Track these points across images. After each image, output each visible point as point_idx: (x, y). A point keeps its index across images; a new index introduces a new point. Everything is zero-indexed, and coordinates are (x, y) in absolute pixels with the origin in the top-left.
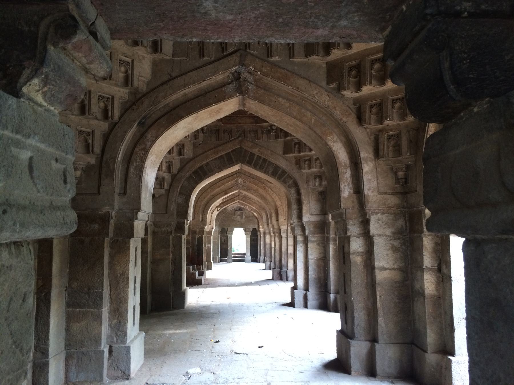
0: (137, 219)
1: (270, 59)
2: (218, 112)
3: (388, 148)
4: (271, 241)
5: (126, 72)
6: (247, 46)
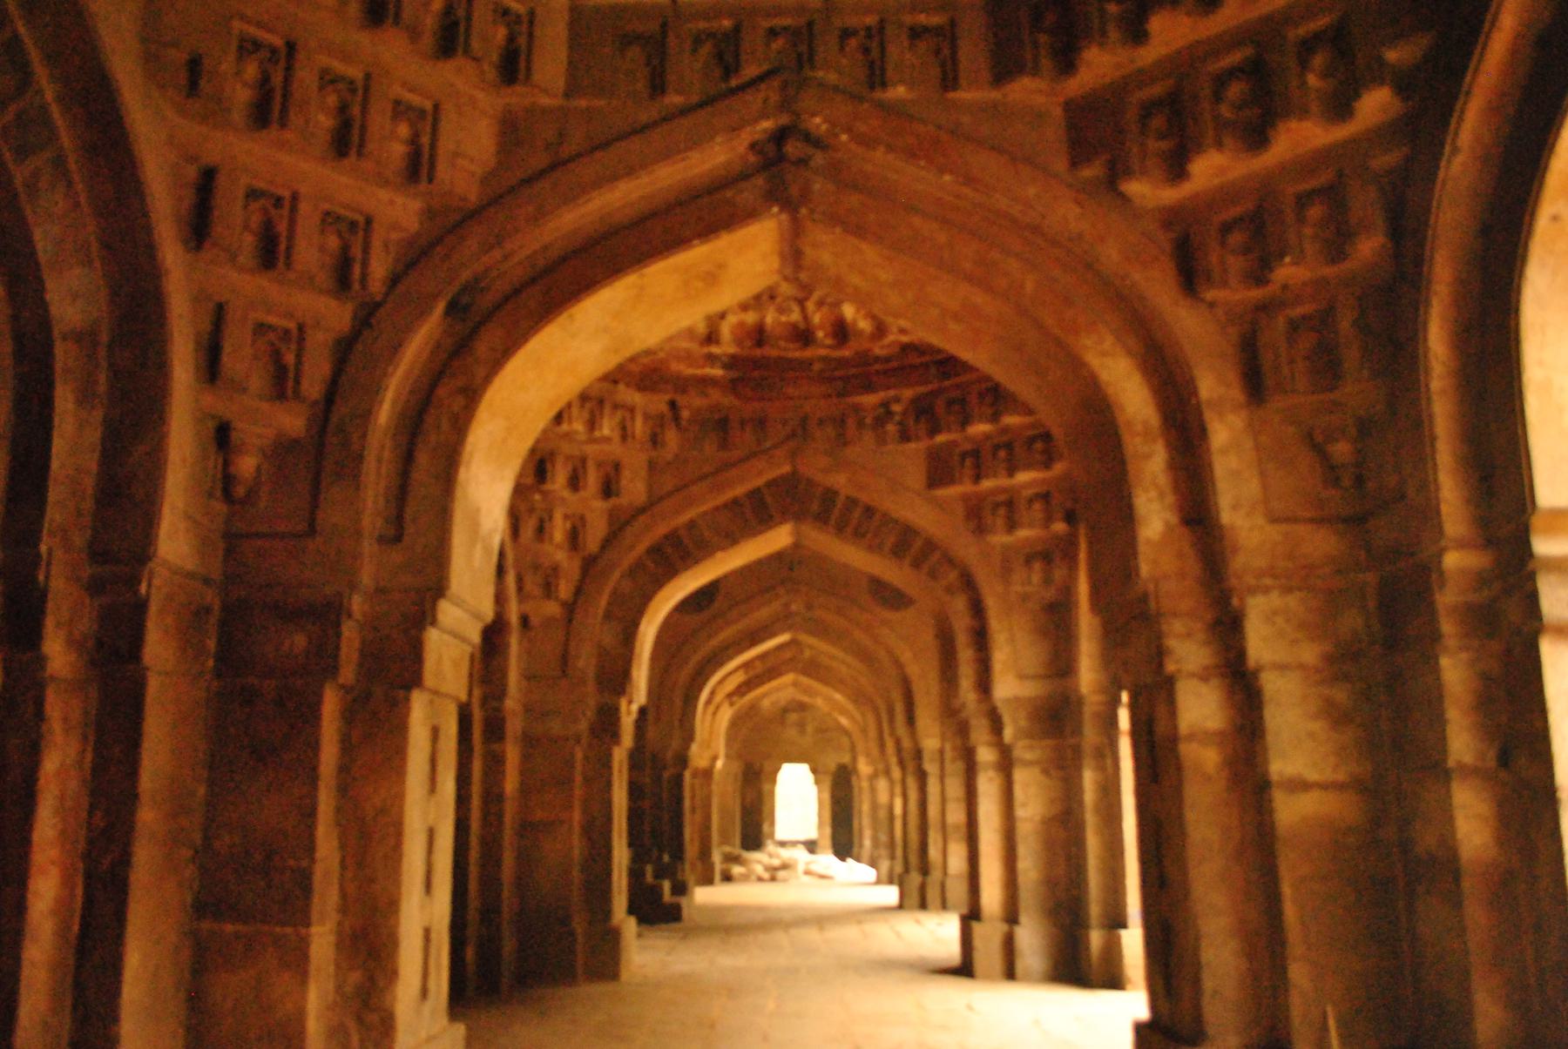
0: (434, 623)
1: (879, 94)
2: (712, 278)
3: (1291, 361)
4: (892, 796)
5: (414, 141)
6: (805, 57)
